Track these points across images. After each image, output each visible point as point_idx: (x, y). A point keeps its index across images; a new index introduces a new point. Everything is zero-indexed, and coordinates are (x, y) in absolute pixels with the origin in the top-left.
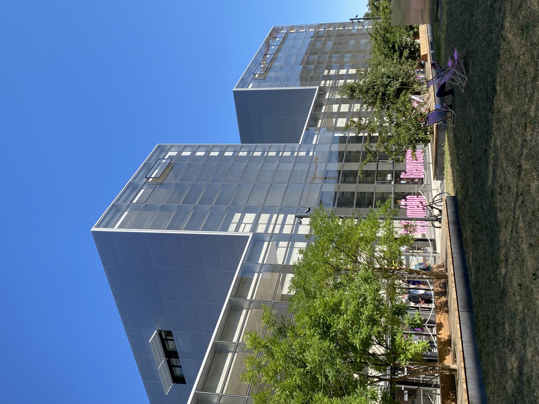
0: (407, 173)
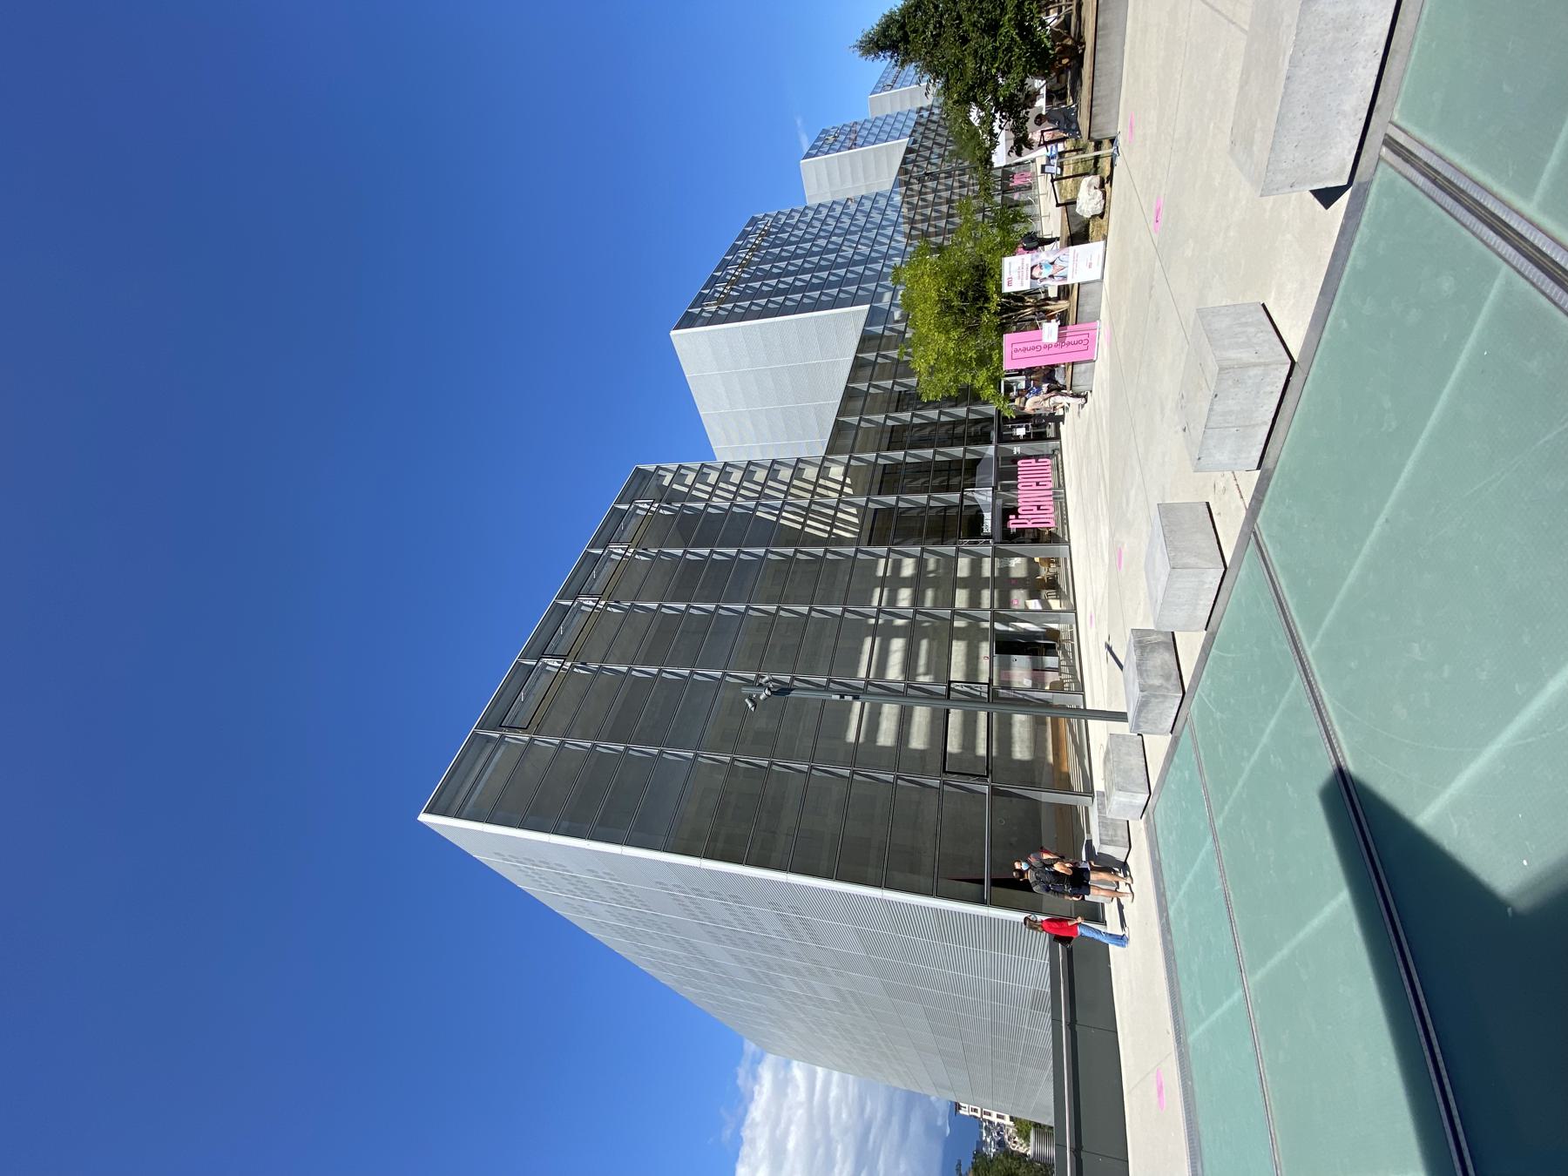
0: (1020, 517)
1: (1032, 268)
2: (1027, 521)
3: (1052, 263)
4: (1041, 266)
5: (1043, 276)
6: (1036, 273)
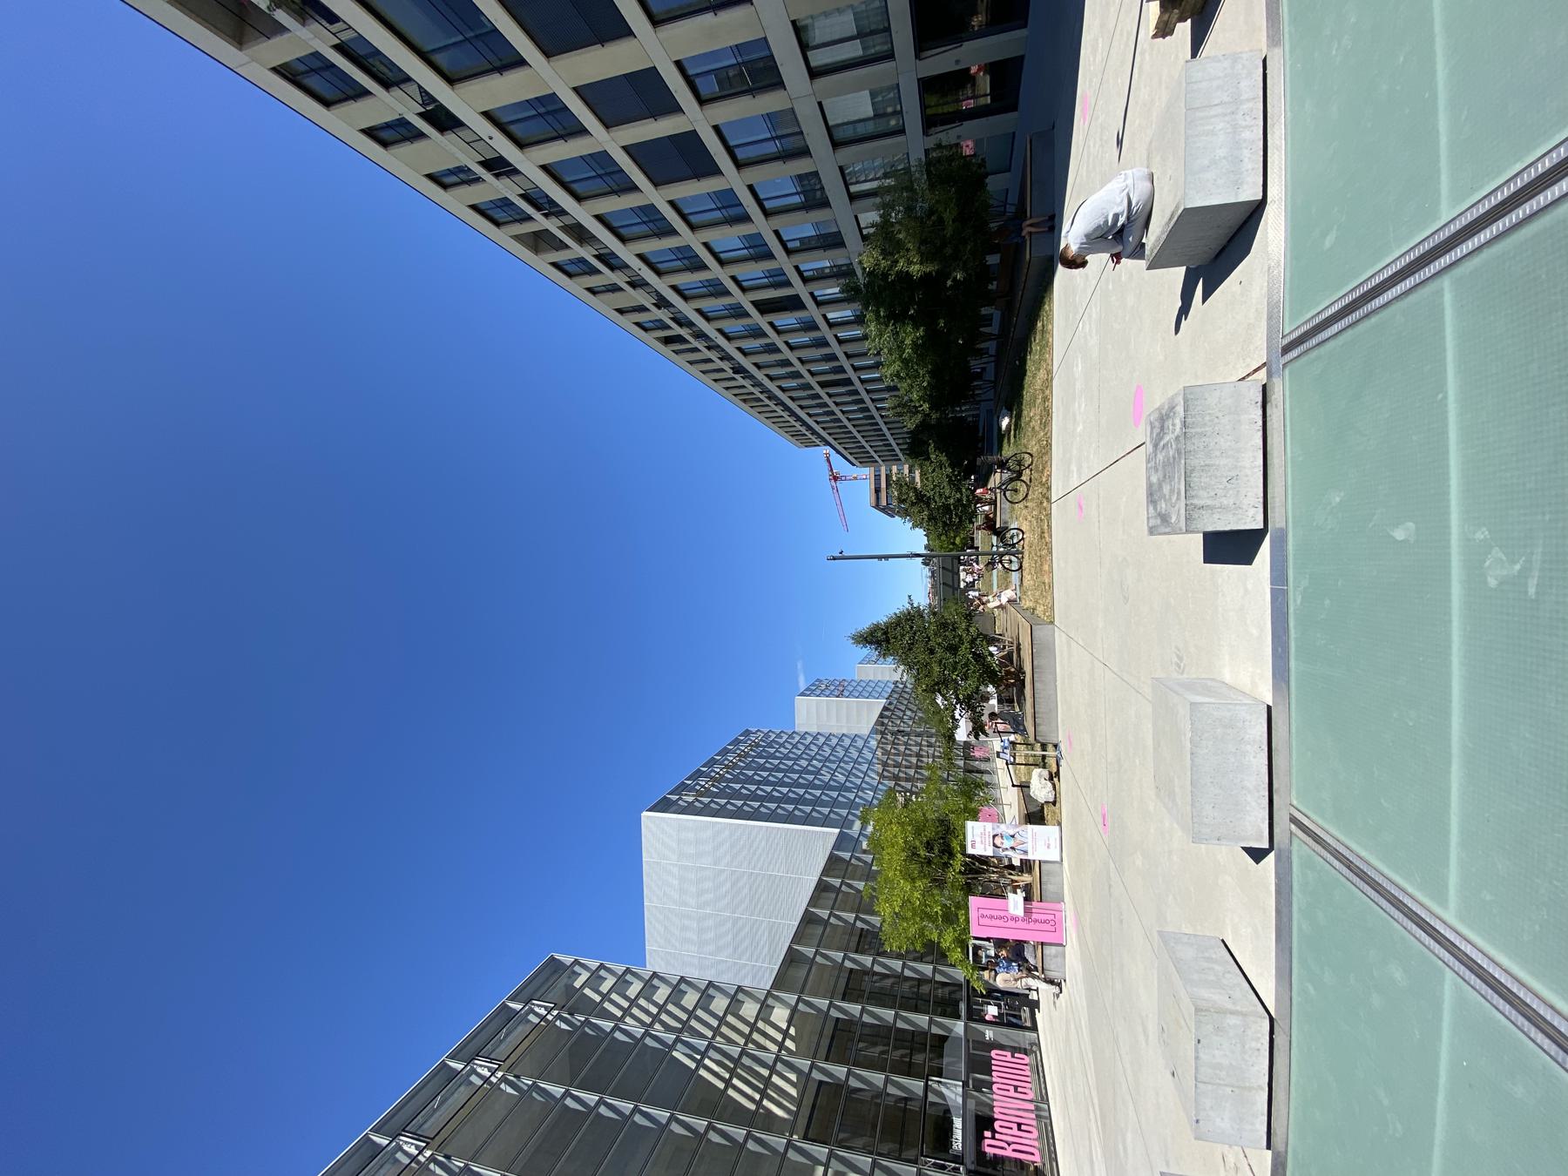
0: (997, 1136)
1: (994, 836)
2: (1006, 1145)
3: (1013, 836)
4: (1002, 837)
5: (1004, 846)
6: (998, 841)
